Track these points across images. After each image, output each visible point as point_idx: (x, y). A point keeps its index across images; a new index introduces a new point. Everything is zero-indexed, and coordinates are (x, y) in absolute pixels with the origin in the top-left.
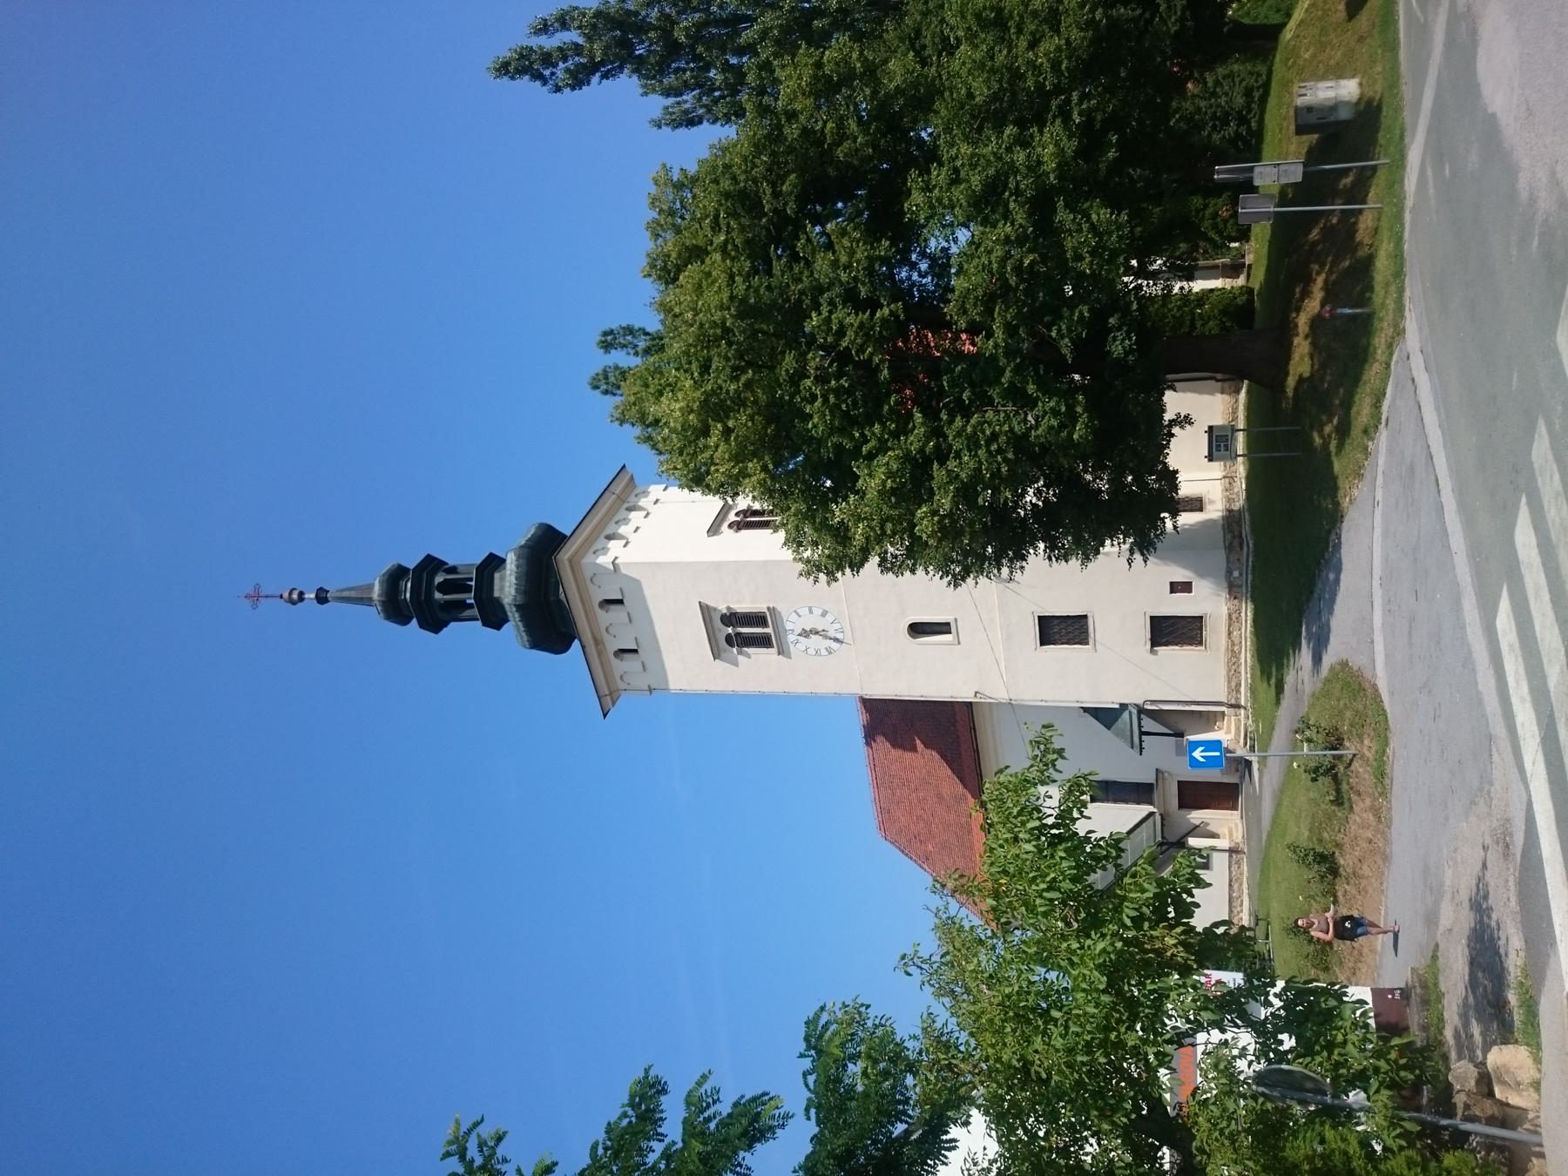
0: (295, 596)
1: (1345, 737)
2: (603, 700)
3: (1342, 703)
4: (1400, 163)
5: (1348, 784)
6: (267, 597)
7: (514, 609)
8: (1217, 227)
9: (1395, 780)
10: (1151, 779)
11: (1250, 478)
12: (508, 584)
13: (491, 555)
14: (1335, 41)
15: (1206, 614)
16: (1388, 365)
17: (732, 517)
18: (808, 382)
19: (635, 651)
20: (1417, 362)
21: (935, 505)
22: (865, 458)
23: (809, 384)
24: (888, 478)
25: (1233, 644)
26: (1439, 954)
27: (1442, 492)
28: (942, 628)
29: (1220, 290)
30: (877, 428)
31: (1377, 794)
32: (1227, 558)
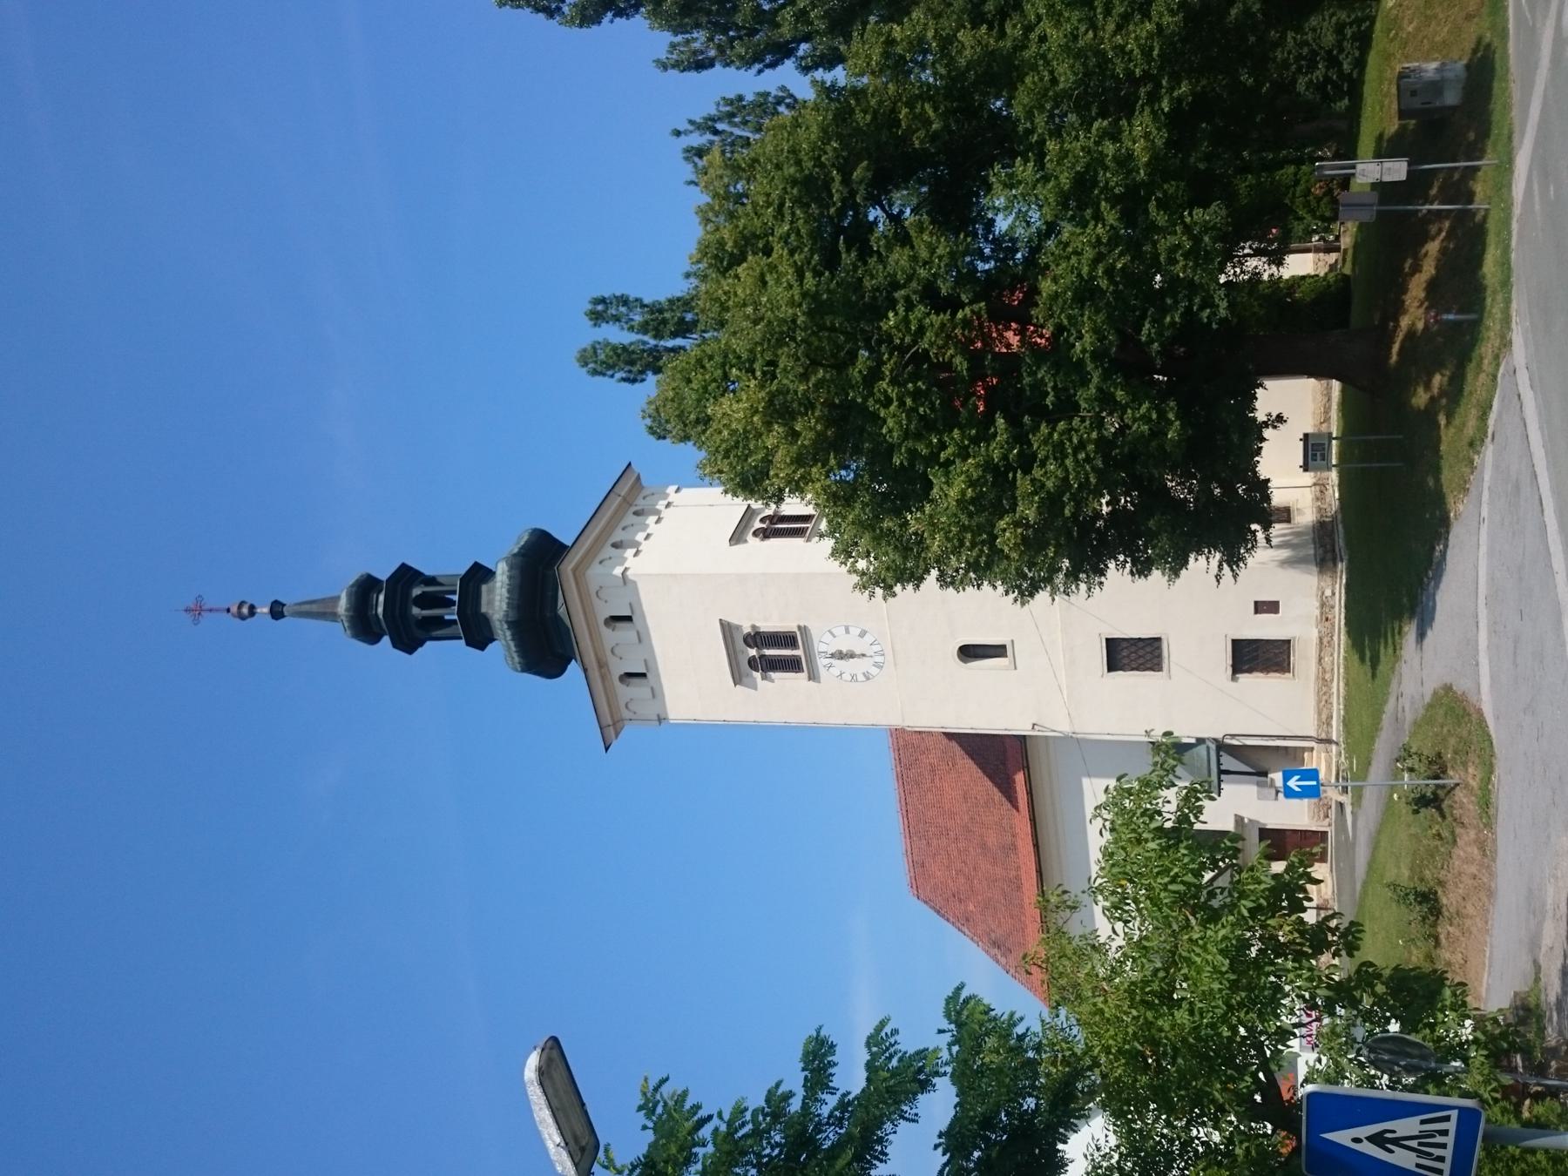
0: (245, 610)
1: (1449, 765)
2: (606, 730)
3: (1445, 730)
4: (1506, 167)
5: (1452, 815)
6: (211, 610)
7: (505, 626)
8: (1310, 206)
9: (1500, 808)
11: (1342, 485)
12: (498, 598)
13: (476, 564)
14: (1441, 16)
15: (1294, 638)
16: (1495, 377)
17: (757, 525)
18: (884, 384)
19: (643, 675)
20: (1523, 378)
21: (1017, 515)
22: (941, 465)
23: (885, 386)
24: (969, 487)
25: (1324, 671)
26: (1541, 976)
27: (1546, 513)
28: (998, 651)
29: (1312, 277)
30: (956, 433)
31: (1482, 826)
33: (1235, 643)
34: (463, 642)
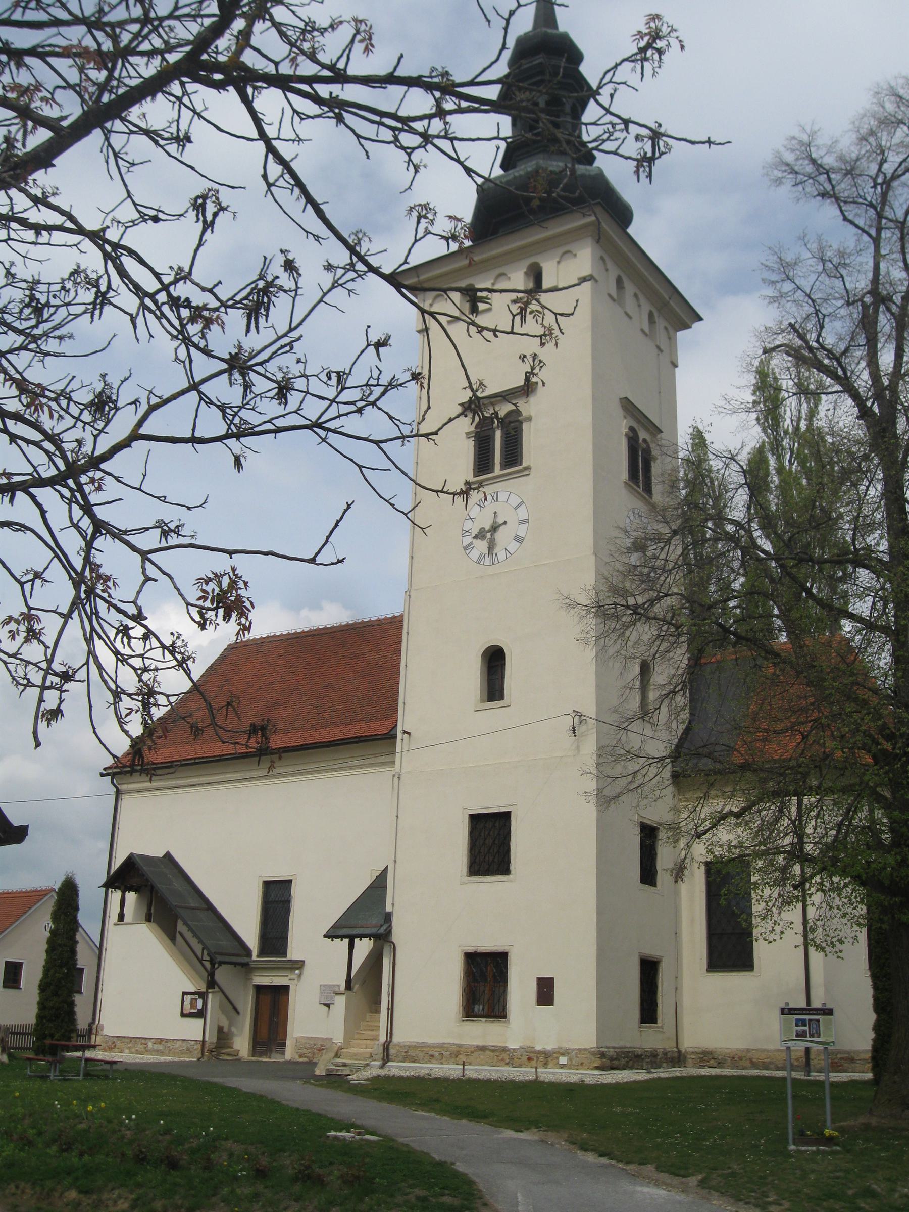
10: (294, 953)
32: (585, 1050)
33: (506, 816)
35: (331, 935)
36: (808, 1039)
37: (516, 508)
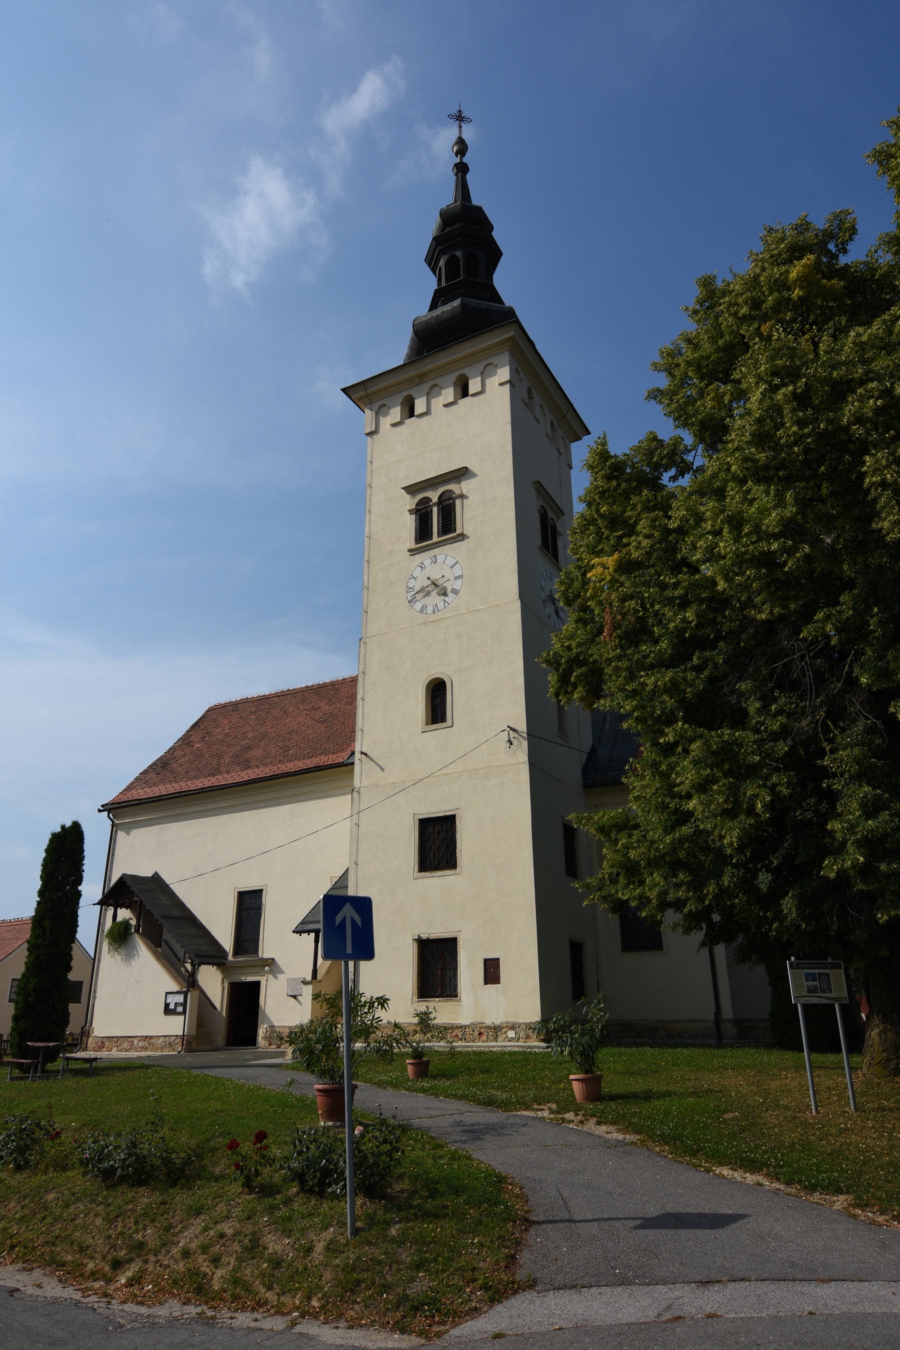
33: (453, 818)
34: (436, 288)
35: (298, 931)
36: (820, 994)
37: (452, 567)
